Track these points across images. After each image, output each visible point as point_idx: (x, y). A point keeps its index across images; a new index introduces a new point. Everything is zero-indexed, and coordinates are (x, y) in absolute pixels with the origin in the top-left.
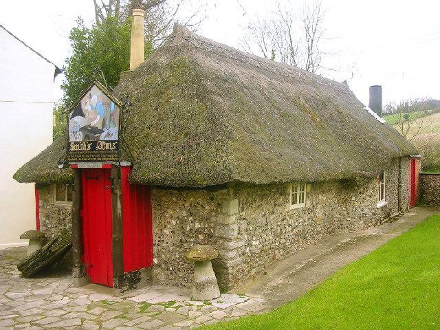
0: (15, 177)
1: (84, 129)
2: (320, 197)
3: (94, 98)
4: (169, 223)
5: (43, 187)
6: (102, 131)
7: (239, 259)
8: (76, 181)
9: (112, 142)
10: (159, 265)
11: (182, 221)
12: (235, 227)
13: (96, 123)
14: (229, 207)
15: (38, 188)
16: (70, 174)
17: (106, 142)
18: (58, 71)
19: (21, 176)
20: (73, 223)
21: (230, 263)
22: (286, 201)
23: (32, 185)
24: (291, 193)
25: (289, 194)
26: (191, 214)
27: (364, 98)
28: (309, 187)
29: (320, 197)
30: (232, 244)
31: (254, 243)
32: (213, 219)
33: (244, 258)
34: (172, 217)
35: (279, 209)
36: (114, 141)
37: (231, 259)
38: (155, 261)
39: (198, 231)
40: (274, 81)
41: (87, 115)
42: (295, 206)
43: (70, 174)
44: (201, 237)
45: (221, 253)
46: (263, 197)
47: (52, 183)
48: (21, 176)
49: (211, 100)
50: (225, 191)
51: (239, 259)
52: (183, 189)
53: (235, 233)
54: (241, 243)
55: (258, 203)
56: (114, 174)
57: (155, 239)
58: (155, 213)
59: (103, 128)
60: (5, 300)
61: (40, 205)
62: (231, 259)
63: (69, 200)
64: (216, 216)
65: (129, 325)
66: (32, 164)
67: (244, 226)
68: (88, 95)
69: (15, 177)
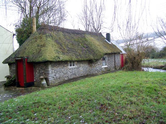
0: (3, 63)
2: (81, 65)
4: (37, 71)
5: (10, 64)
8: (16, 62)
10: (35, 81)
11: (40, 71)
12: (51, 71)
18: (14, 35)
19: (5, 62)
20: (16, 74)
21: (50, 79)
22: (68, 66)
23: (7, 64)
25: (69, 64)
26: (41, 69)
27: (105, 35)
28: (76, 63)
29: (81, 65)
30: (50, 75)
31: (57, 75)
32: (45, 70)
33: (54, 78)
34: (37, 70)
37: (50, 78)
38: (35, 80)
42: (71, 67)
45: (47, 77)
46: (59, 64)
48: (5, 62)
50: (47, 63)
51: (52, 79)
52: (39, 63)
53: (51, 73)
54: (52, 75)
56: (23, 60)
57: (35, 75)
58: (34, 69)
62: (50, 78)
64: (46, 69)
65: (10, 36)
66: (7, 59)
67: (53, 71)
69: (3, 63)
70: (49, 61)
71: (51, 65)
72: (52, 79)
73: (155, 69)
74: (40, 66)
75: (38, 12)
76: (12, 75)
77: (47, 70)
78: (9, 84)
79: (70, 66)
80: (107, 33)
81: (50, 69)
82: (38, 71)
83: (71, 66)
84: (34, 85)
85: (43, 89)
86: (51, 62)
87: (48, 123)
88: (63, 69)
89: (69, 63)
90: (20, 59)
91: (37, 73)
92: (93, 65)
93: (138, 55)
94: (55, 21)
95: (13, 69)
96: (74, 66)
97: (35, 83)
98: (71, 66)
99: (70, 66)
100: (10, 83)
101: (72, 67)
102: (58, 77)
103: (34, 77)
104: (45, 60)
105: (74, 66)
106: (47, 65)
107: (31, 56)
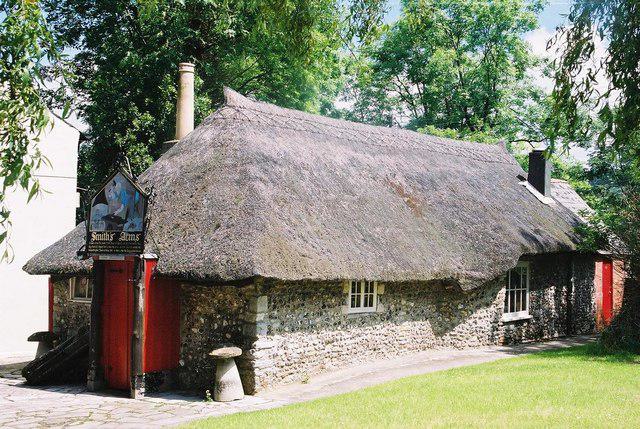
1: (106, 218)
2: (404, 302)
3: (119, 185)
4: (198, 321)
6: (126, 221)
7: (267, 360)
9: (136, 233)
10: (185, 367)
13: (120, 212)
14: (255, 304)
15: (52, 281)
16: (88, 264)
17: (130, 233)
22: (344, 303)
23: (46, 329)
24: (350, 294)
35: (331, 312)
36: (138, 233)
39: (227, 329)
40: (359, 156)
41: (110, 203)
42: (356, 310)
43: (88, 264)
44: (228, 336)
47: (70, 275)
49: (251, 189)
55: (298, 301)
59: (127, 216)
60: (6, 402)
61: (55, 302)
63: (89, 296)
68: (111, 182)
70: (309, 281)
71: (265, 298)
72: (271, 362)
73: (317, 284)
79: (366, 305)
80: (534, 151)
81: (260, 317)
82: (202, 320)
83: (358, 305)
86: (269, 285)
88: (318, 320)
92: (460, 307)
94: (8, 30)
96: (371, 305)
98: (358, 305)
99: (366, 305)
101: (362, 309)
102: (294, 355)
103: (182, 349)
105: (371, 305)
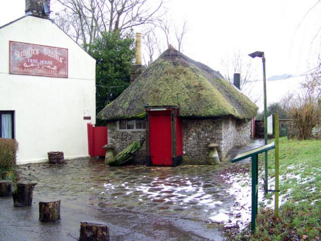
10: (186, 154)
11: (199, 134)
26: (203, 130)
32: (214, 132)
38: (184, 152)
74: (200, 124)
75: (83, 30)
76: (117, 144)
77: (218, 131)
78: (124, 160)
84: (183, 162)
85: (60, 168)
87: (166, 239)
89: (118, 123)
90: (165, 109)
91: (190, 139)
93: (308, 106)
95: (118, 132)
97: (185, 158)
100: (126, 159)
103: (184, 147)
104: (224, 113)
106: (218, 124)
107: (183, 106)
